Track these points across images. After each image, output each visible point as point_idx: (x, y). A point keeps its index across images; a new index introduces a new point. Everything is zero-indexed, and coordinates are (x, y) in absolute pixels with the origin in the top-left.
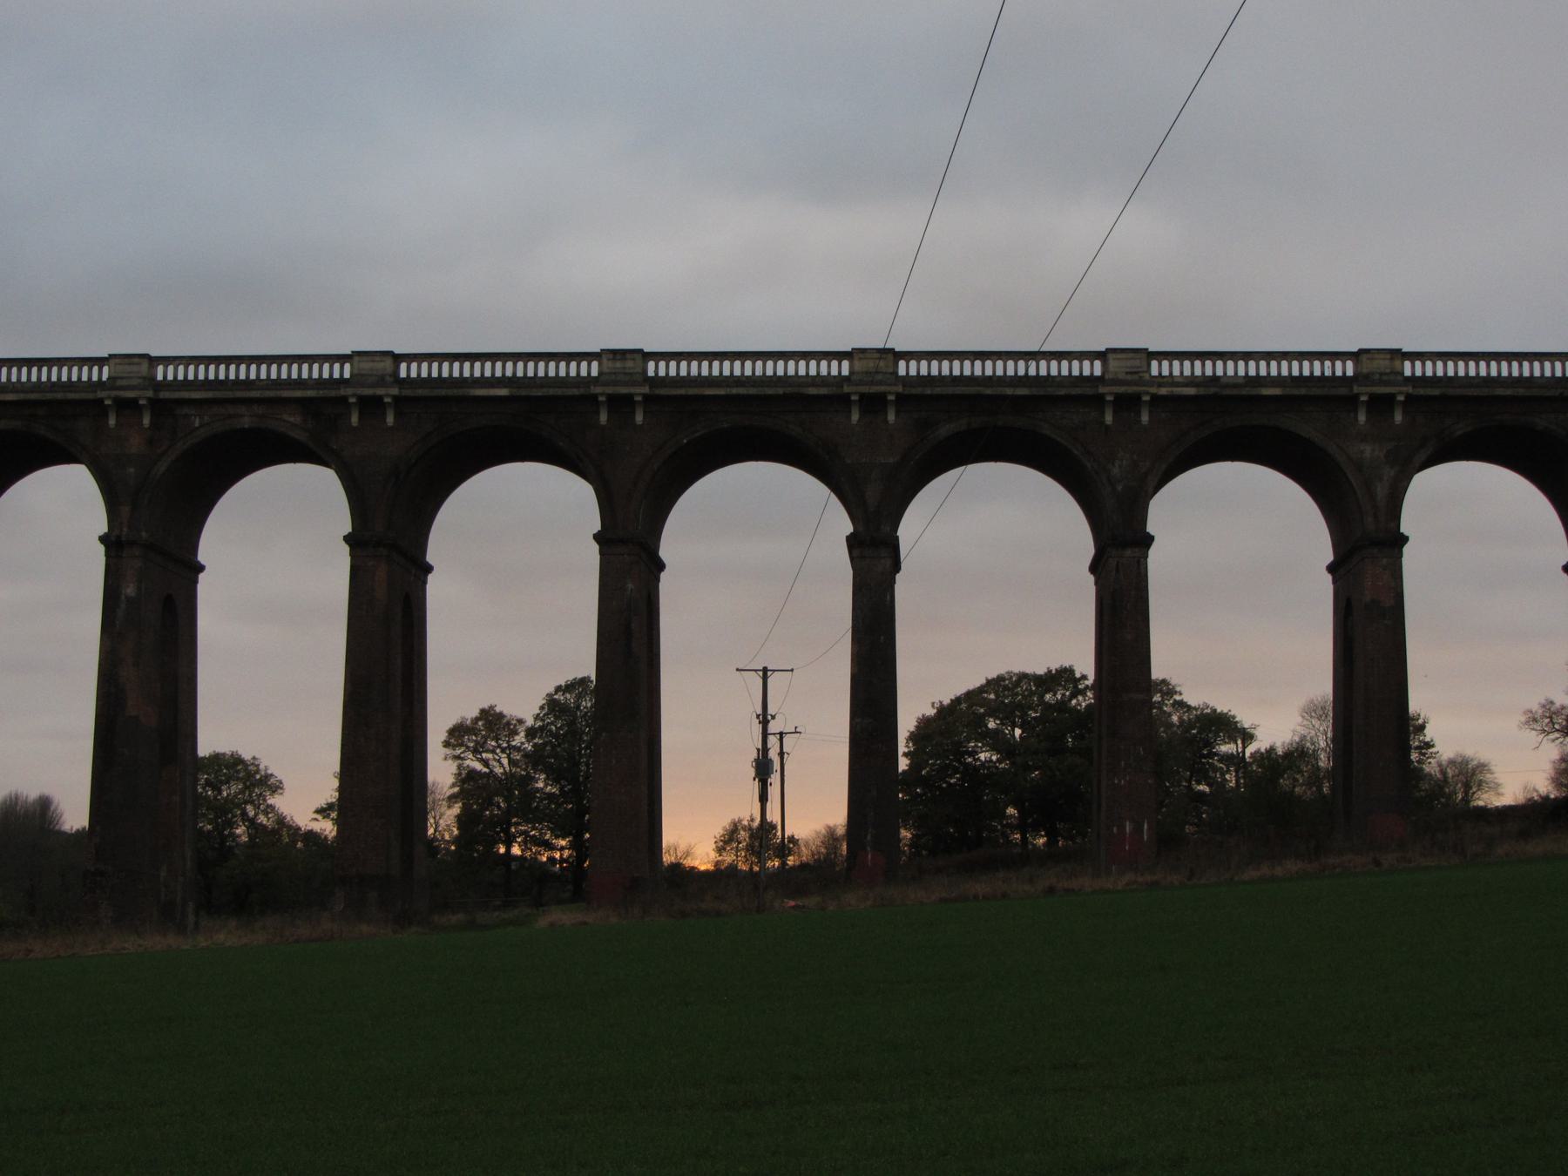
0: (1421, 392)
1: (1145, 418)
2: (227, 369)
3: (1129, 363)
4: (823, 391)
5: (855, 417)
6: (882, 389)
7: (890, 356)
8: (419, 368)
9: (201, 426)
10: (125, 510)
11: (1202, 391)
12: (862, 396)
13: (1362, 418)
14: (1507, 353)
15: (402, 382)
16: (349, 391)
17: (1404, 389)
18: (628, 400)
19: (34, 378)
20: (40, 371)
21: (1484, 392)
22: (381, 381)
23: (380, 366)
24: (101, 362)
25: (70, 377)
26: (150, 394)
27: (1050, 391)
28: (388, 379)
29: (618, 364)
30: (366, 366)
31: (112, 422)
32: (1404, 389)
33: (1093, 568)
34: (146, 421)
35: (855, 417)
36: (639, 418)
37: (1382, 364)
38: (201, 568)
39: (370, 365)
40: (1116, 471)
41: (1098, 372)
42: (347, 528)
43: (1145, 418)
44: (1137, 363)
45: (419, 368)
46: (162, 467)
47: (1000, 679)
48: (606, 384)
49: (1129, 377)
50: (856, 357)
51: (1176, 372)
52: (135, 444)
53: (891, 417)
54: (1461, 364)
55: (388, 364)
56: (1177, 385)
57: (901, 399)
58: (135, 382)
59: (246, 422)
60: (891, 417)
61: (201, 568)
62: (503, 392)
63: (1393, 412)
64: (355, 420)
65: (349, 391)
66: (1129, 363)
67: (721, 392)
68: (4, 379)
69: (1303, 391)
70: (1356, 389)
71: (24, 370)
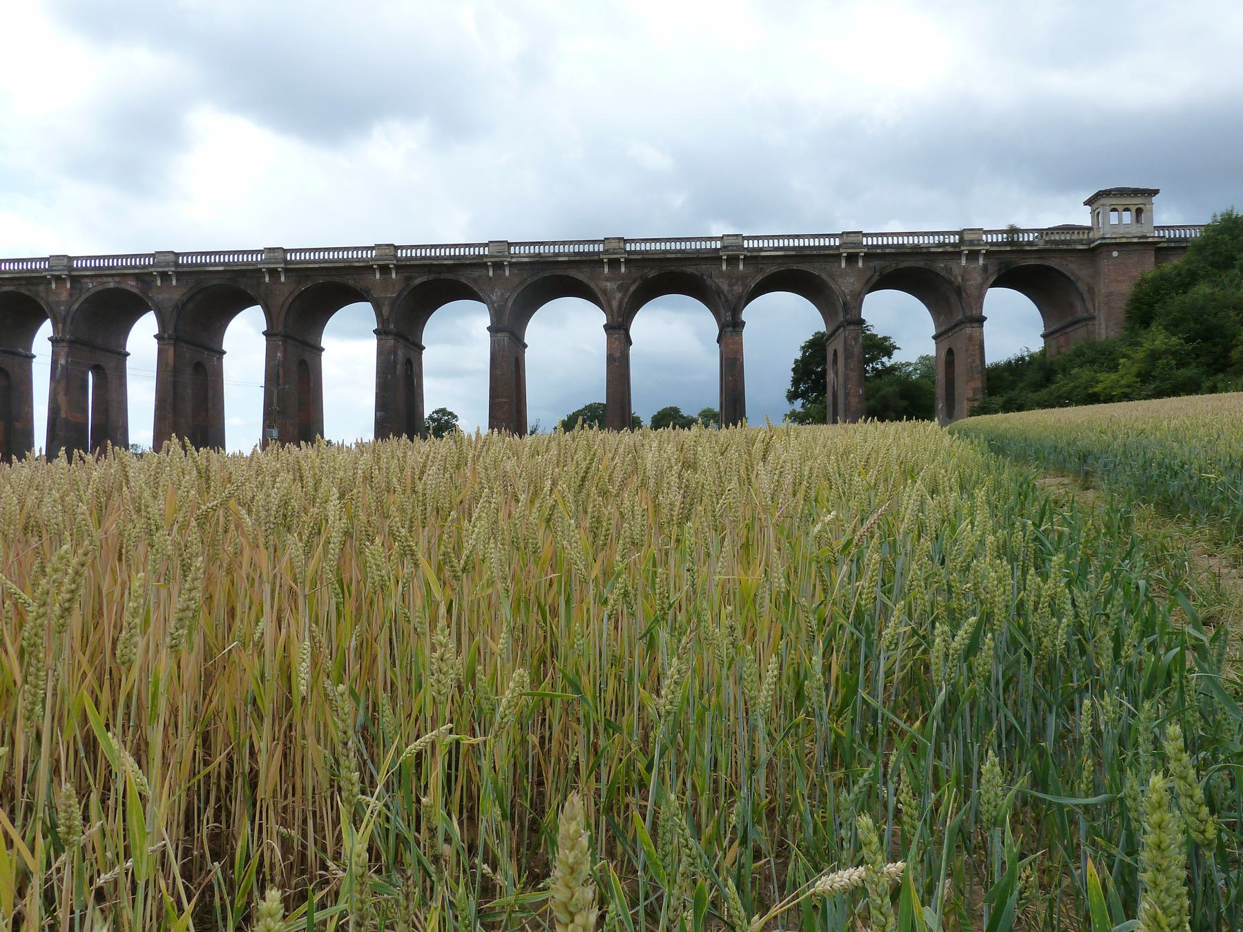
0: (995, 249)
1: (507, 273)
2: (310, 255)
3: (499, 248)
4: (893, 251)
5: (378, 276)
6: (387, 262)
7: (392, 248)
8: (411, 252)
9: (93, 287)
10: (60, 326)
11: (531, 260)
12: (609, 259)
13: (606, 270)
14: (871, 234)
15: (398, 259)
16: (153, 270)
17: (864, 250)
18: (617, 261)
19: (552, 251)
20: (305, 255)
21: (662, 256)
22: (168, 265)
23: (167, 258)
24: (371, 248)
25: (187, 262)
26: (283, 265)
27: (463, 261)
28: (171, 264)
29: (272, 254)
30: (162, 258)
31: (54, 286)
32: (864, 250)
33: (718, 342)
34: (68, 286)
35: (378, 276)
36: (283, 279)
37: (614, 245)
38: (323, 350)
39: (163, 258)
40: (494, 298)
41: (719, 246)
42: (156, 332)
43: (507, 273)
44: (502, 247)
45: (411, 252)
46: (76, 307)
47: (591, 405)
48: (265, 263)
49: (499, 254)
50: (606, 242)
51: (522, 252)
52: (64, 296)
53: (394, 276)
54: (890, 238)
55: (171, 258)
56: (520, 257)
57: (398, 267)
58: (60, 268)
59: (112, 285)
60: (394, 276)
61: (323, 350)
62: (221, 268)
63: (961, 259)
64: (159, 283)
65: (153, 270)
66: (499, 248)
67: (317, 266)
68: (75, 266)
69: (578, 258)
70: (841, 251)
71: (365, 252)
